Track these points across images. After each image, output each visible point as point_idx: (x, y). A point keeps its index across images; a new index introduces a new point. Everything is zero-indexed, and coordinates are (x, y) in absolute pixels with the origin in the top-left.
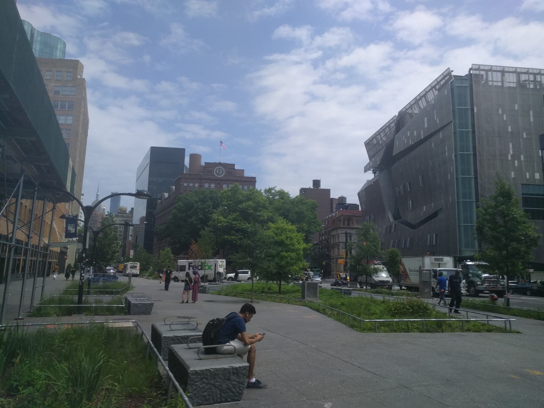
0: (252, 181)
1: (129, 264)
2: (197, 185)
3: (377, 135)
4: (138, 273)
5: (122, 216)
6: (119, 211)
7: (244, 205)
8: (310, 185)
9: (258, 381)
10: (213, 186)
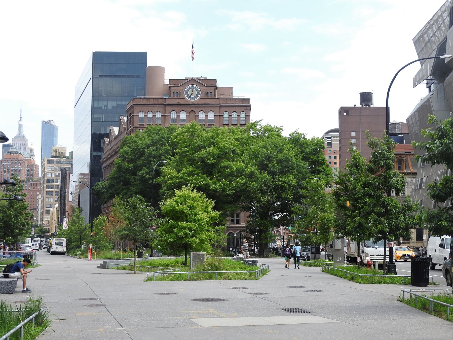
0: (245, 105)
1: (54, 241)
2: (158, 115)
3: (428, 29)
4: (65, 250)
5: (59, 162)
6: (54, 154)
7: (203, 153)
8: (355, 101)
9: (27, 289)
10: (183, 115)
